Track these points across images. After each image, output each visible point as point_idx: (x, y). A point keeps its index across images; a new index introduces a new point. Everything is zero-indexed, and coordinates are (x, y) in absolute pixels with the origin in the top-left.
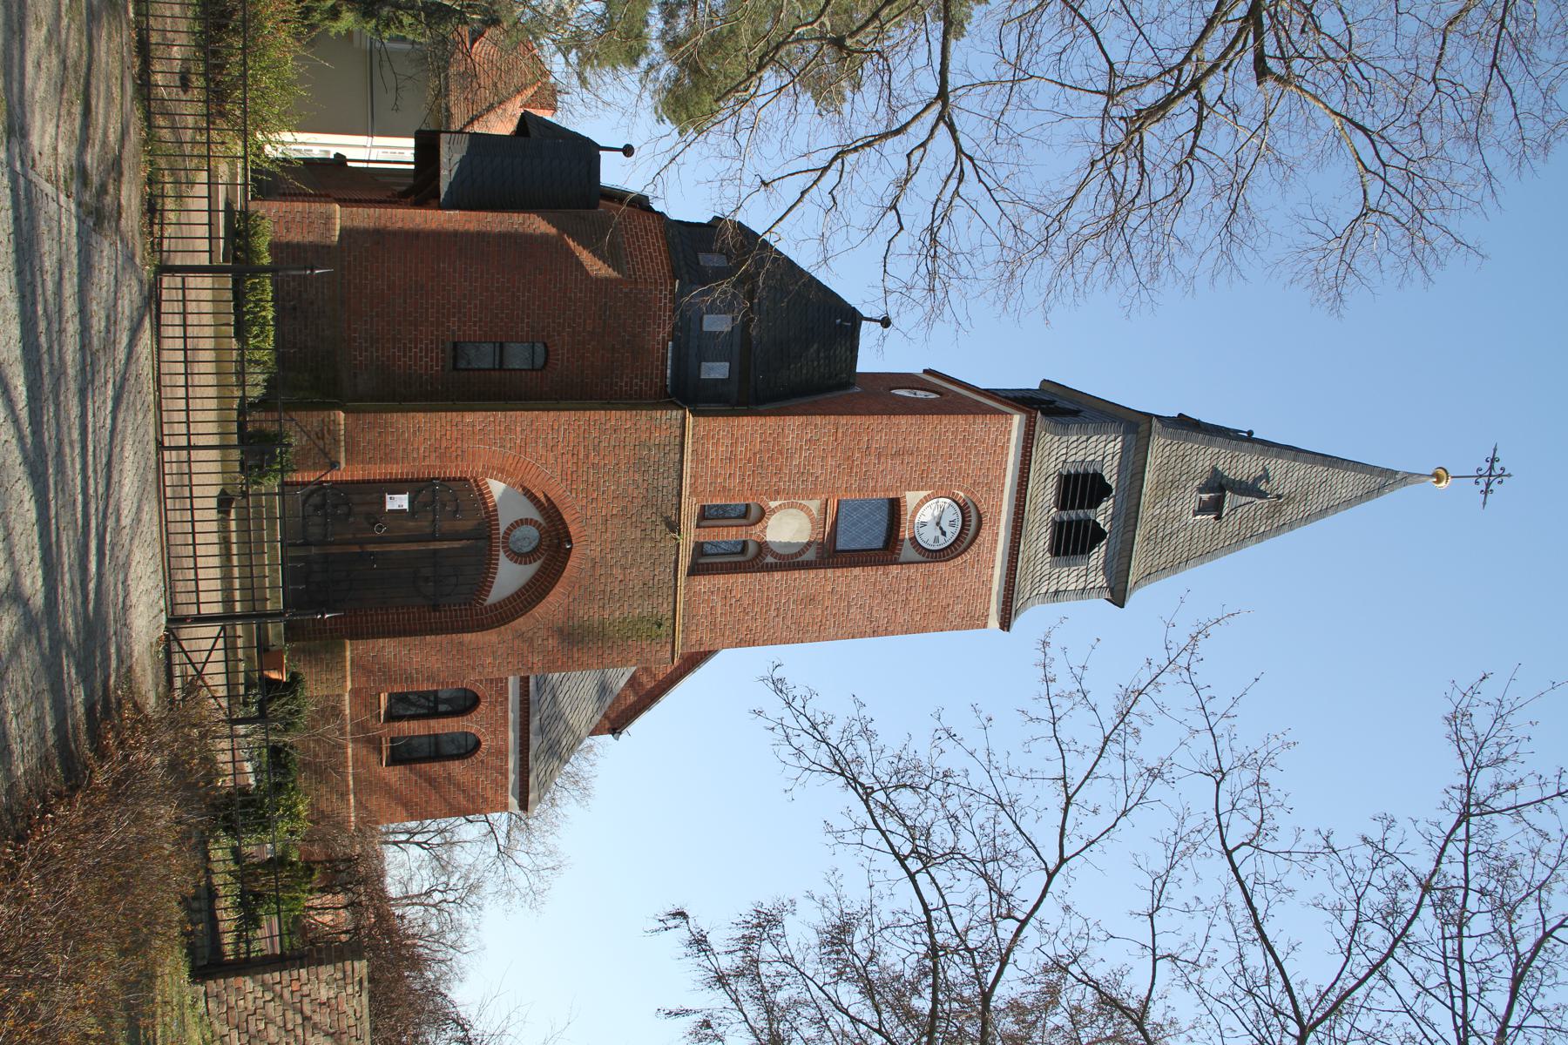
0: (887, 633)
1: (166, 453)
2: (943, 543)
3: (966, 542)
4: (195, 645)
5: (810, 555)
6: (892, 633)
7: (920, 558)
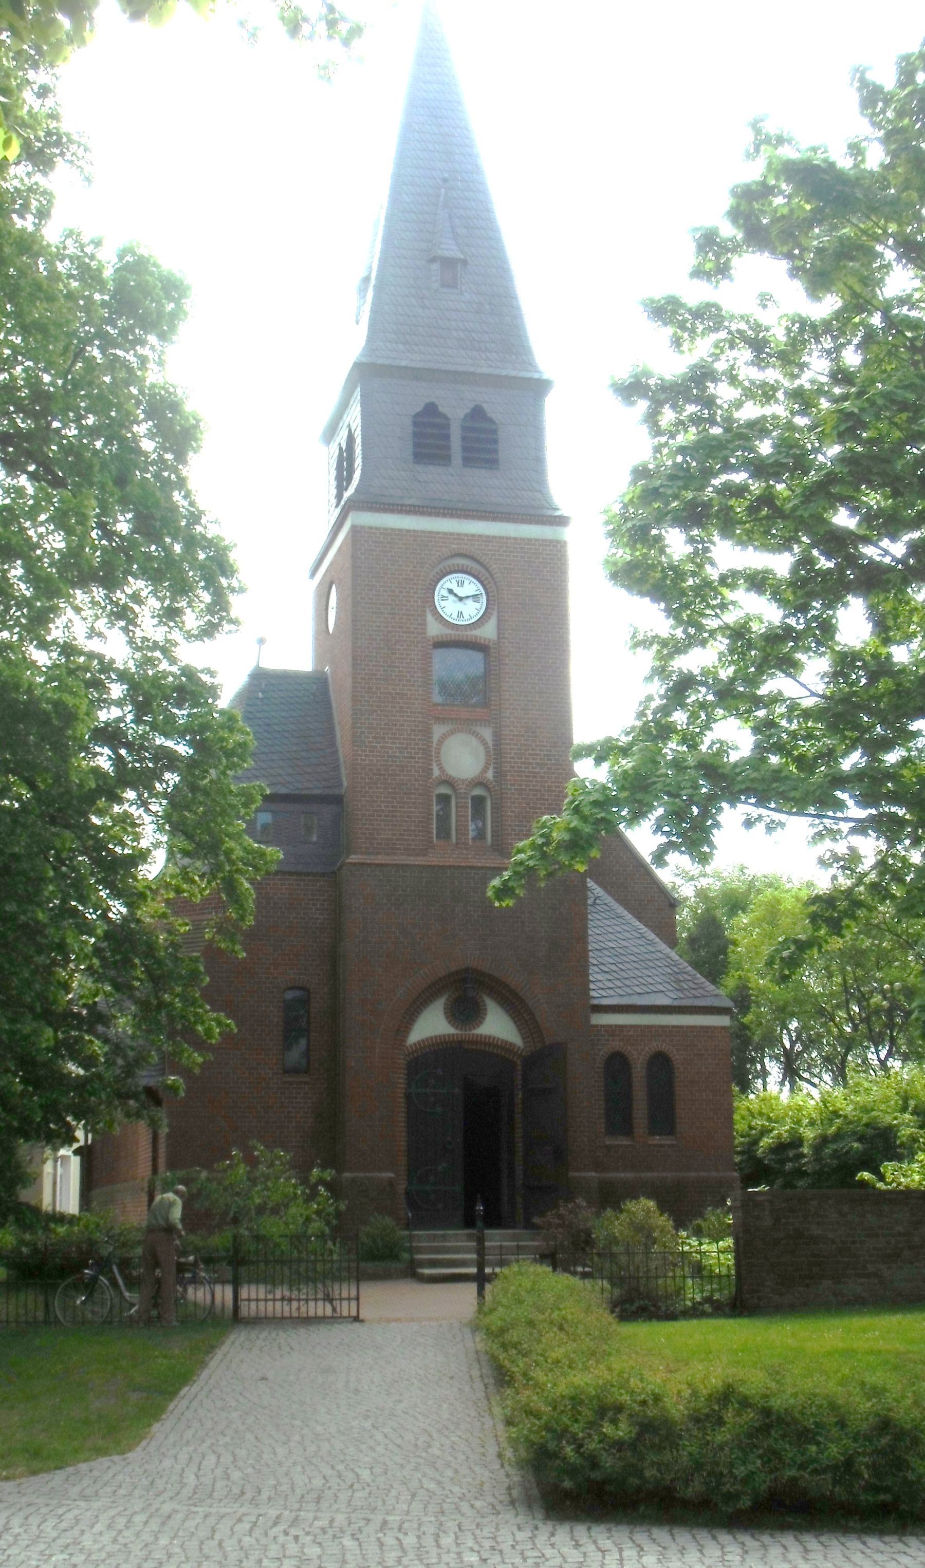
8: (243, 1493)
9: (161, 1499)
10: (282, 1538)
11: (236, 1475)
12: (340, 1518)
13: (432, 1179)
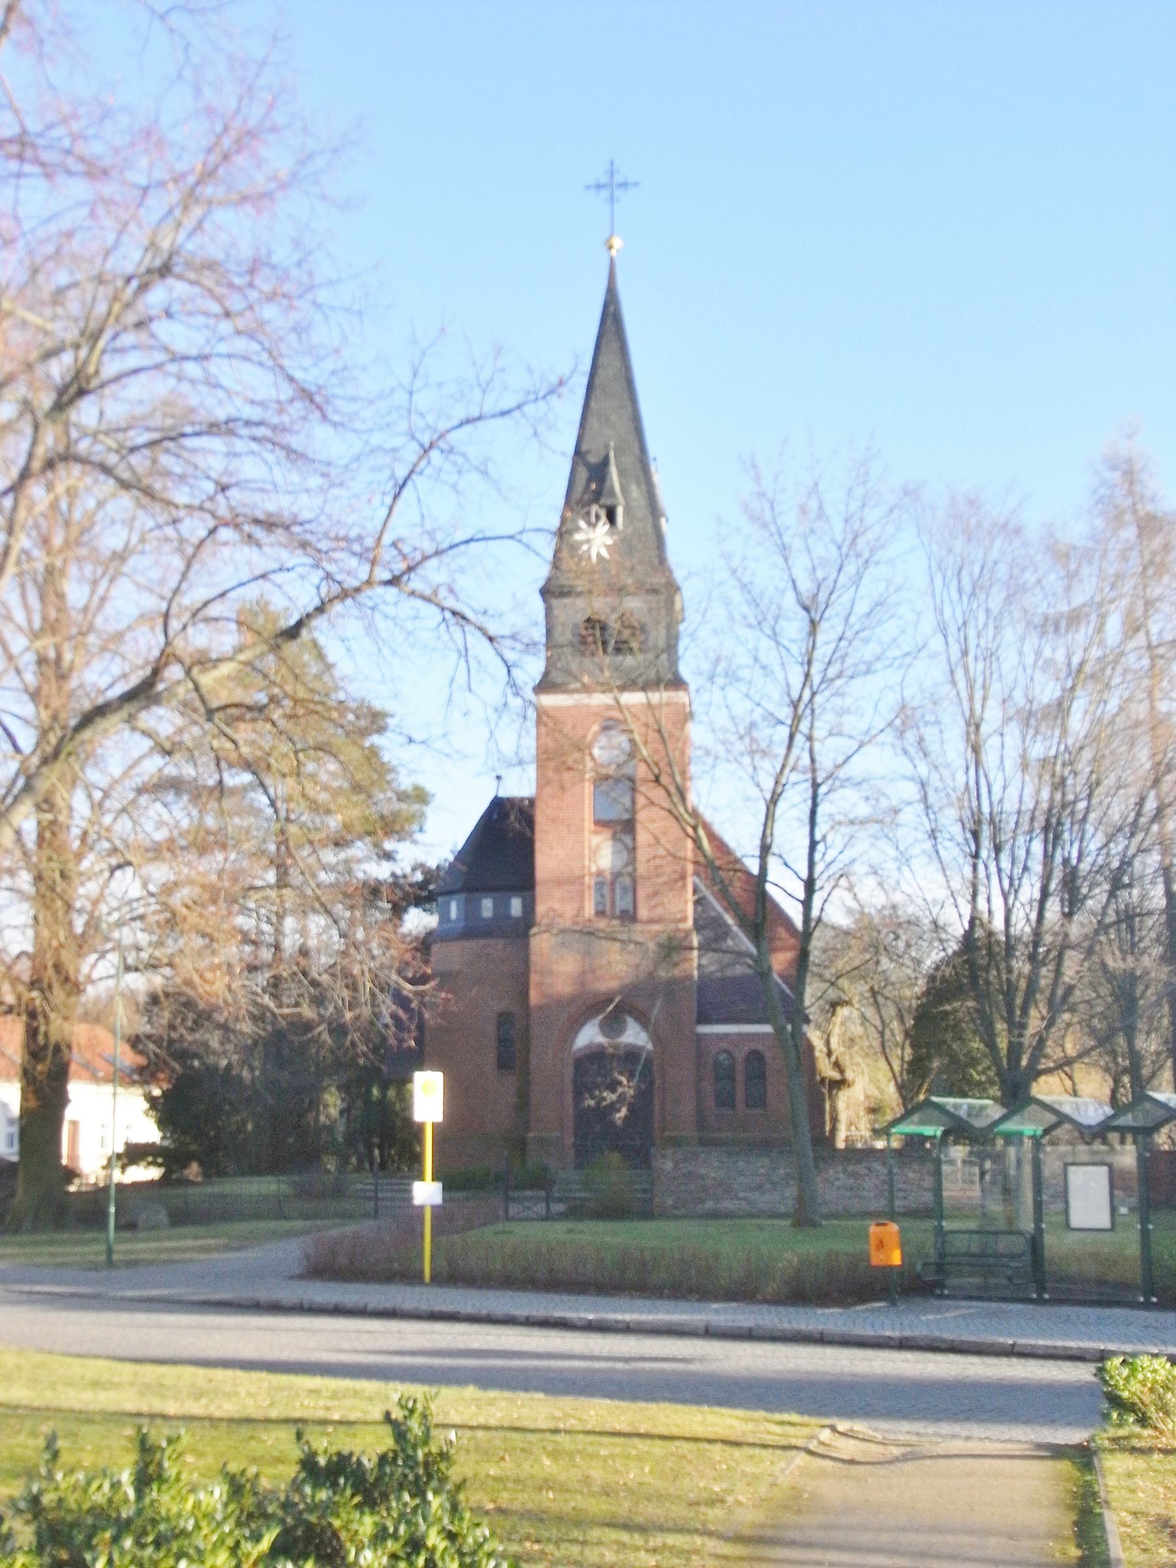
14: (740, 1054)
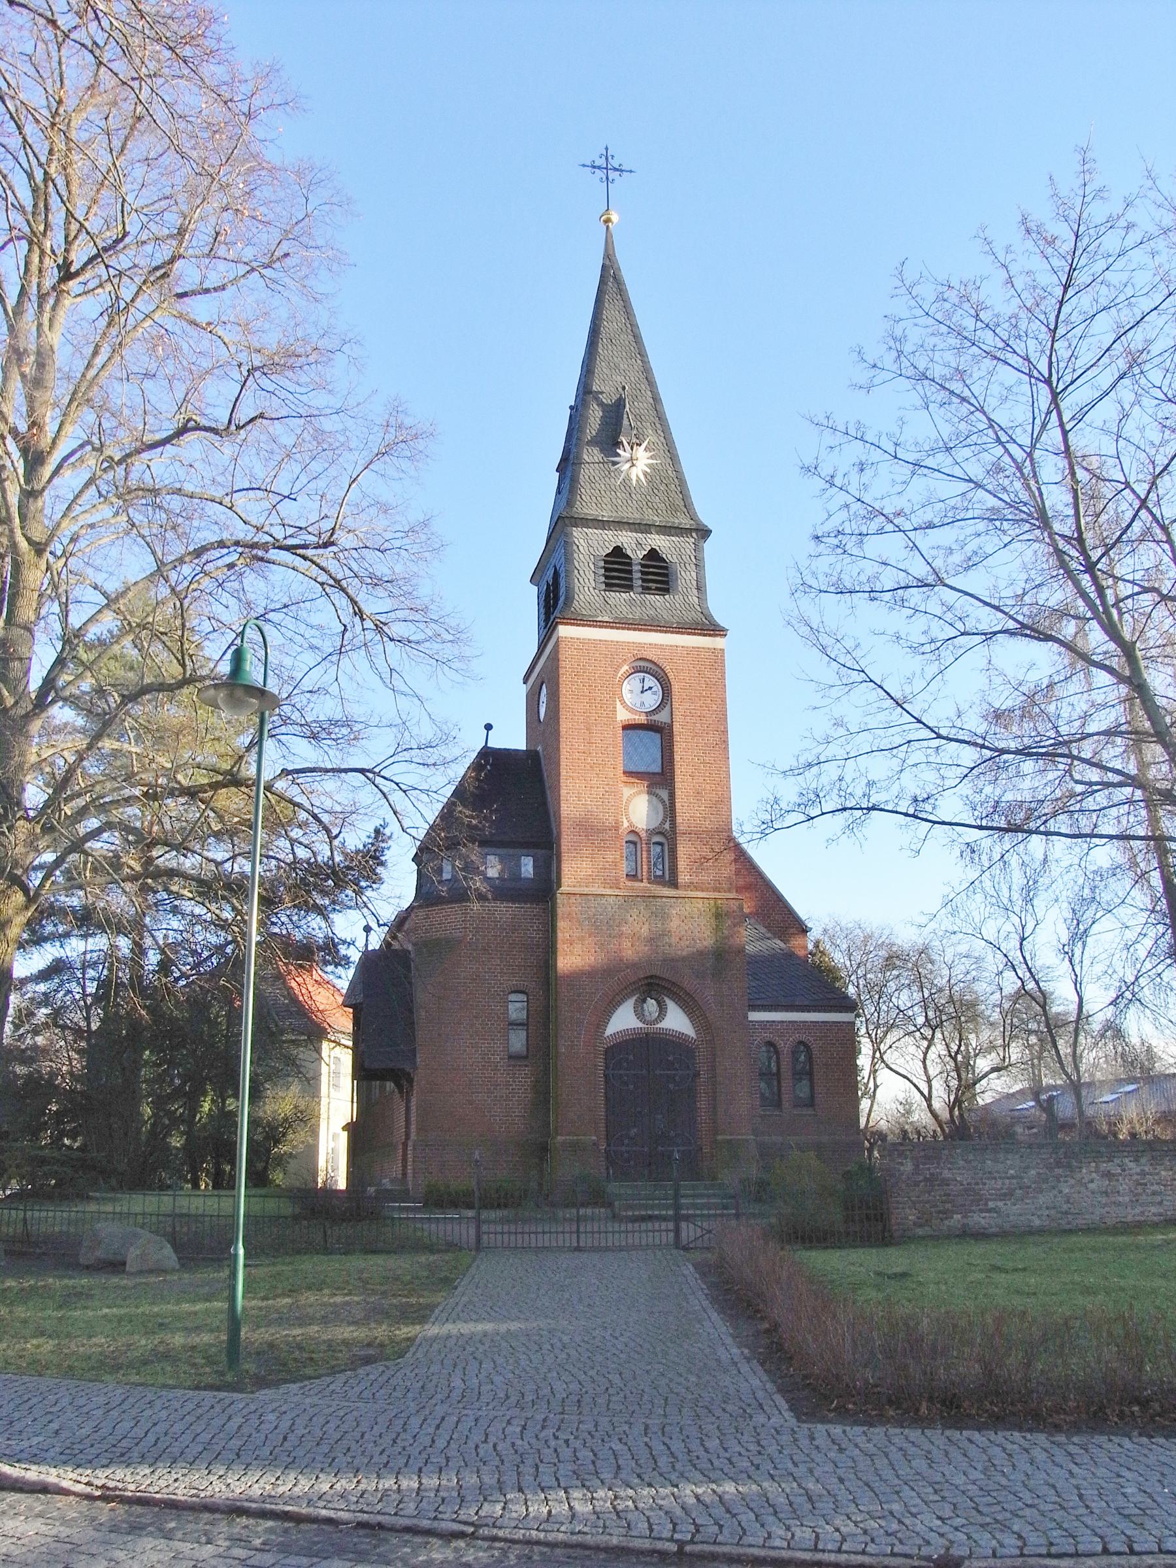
0: (725, 732)
1: (581, 1244)
2: (657, 688)
3: (654, 667)
4: (692, 1233)
5: (664, 794)
6: (726, 728)
7: (668, 707)
8: (508, 1397)
9: (433, 1401)
10: (553, 1443)
11: (498, 1379)
12: (604, 1422)
13: (626, 1141)
14: (785, 1046)
